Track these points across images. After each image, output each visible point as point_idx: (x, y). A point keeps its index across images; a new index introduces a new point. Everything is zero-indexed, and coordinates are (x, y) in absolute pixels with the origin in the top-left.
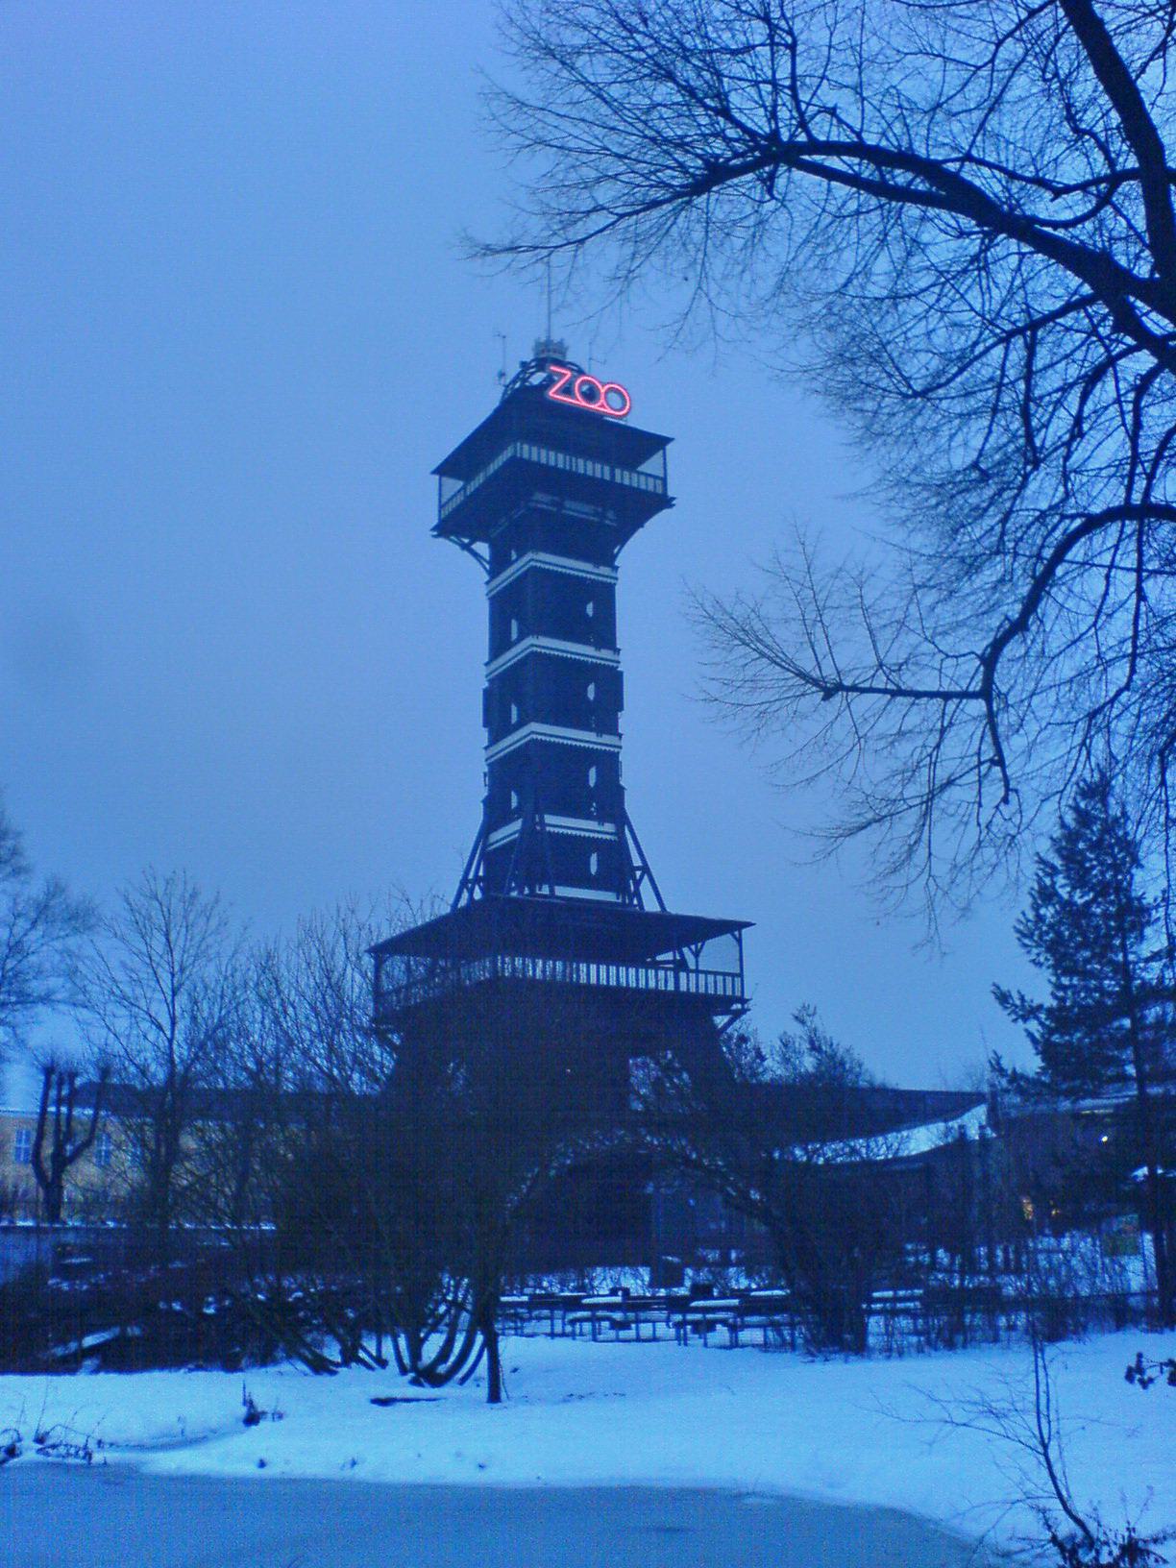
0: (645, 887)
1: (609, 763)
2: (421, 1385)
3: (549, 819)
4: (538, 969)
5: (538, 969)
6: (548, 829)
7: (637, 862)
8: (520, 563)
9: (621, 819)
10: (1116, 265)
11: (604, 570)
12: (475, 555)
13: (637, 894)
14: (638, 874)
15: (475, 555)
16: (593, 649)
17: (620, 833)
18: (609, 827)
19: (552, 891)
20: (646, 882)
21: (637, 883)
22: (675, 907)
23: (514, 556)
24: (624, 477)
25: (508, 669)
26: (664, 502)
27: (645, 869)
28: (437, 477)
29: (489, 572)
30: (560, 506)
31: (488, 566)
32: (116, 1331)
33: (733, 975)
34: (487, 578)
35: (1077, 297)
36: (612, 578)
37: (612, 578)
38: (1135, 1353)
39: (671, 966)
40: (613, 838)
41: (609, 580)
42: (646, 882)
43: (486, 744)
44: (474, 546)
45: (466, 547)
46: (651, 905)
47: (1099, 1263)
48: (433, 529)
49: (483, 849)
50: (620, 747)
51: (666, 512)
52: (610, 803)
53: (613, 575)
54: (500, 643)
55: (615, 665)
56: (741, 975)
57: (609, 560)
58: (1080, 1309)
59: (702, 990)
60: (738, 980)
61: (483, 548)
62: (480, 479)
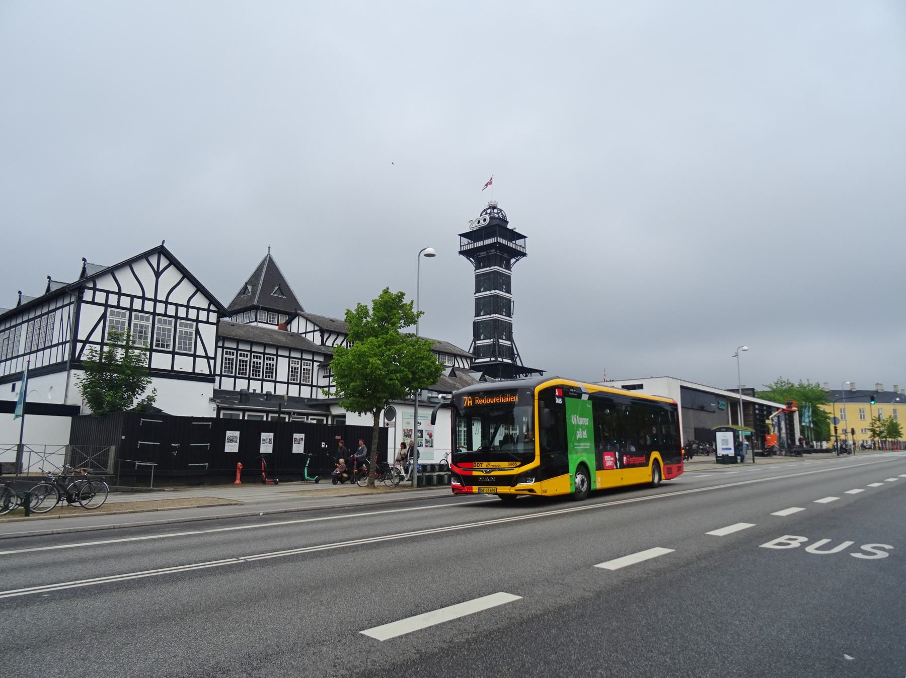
0: (518, 360)
2: (486, 381)
4: (308, 462)
5: (308, 462)
6: (500, 343)
7: (516, 353)
8: (484, 293)
13: (516, 361)
14: (516, 356)
17: (512, 345)
18: (510, 343)
20: (518, 358)
21: (516, 358)
22: (525, 365)
23: (482, 290)
24: (511, 245)
25: (487, 345)
26: (524, 255)
27: (518, 355)
29: (475, 267)
32: (306, 468)
38: (412, 299)
39: (570, 394)
42: (518, 358)
43: (474, 292)
45: (468, 259)
46: (519, 364)
49: (475, 347)
52: (510, 338)
54: (478, 291)
57: (508, 267)
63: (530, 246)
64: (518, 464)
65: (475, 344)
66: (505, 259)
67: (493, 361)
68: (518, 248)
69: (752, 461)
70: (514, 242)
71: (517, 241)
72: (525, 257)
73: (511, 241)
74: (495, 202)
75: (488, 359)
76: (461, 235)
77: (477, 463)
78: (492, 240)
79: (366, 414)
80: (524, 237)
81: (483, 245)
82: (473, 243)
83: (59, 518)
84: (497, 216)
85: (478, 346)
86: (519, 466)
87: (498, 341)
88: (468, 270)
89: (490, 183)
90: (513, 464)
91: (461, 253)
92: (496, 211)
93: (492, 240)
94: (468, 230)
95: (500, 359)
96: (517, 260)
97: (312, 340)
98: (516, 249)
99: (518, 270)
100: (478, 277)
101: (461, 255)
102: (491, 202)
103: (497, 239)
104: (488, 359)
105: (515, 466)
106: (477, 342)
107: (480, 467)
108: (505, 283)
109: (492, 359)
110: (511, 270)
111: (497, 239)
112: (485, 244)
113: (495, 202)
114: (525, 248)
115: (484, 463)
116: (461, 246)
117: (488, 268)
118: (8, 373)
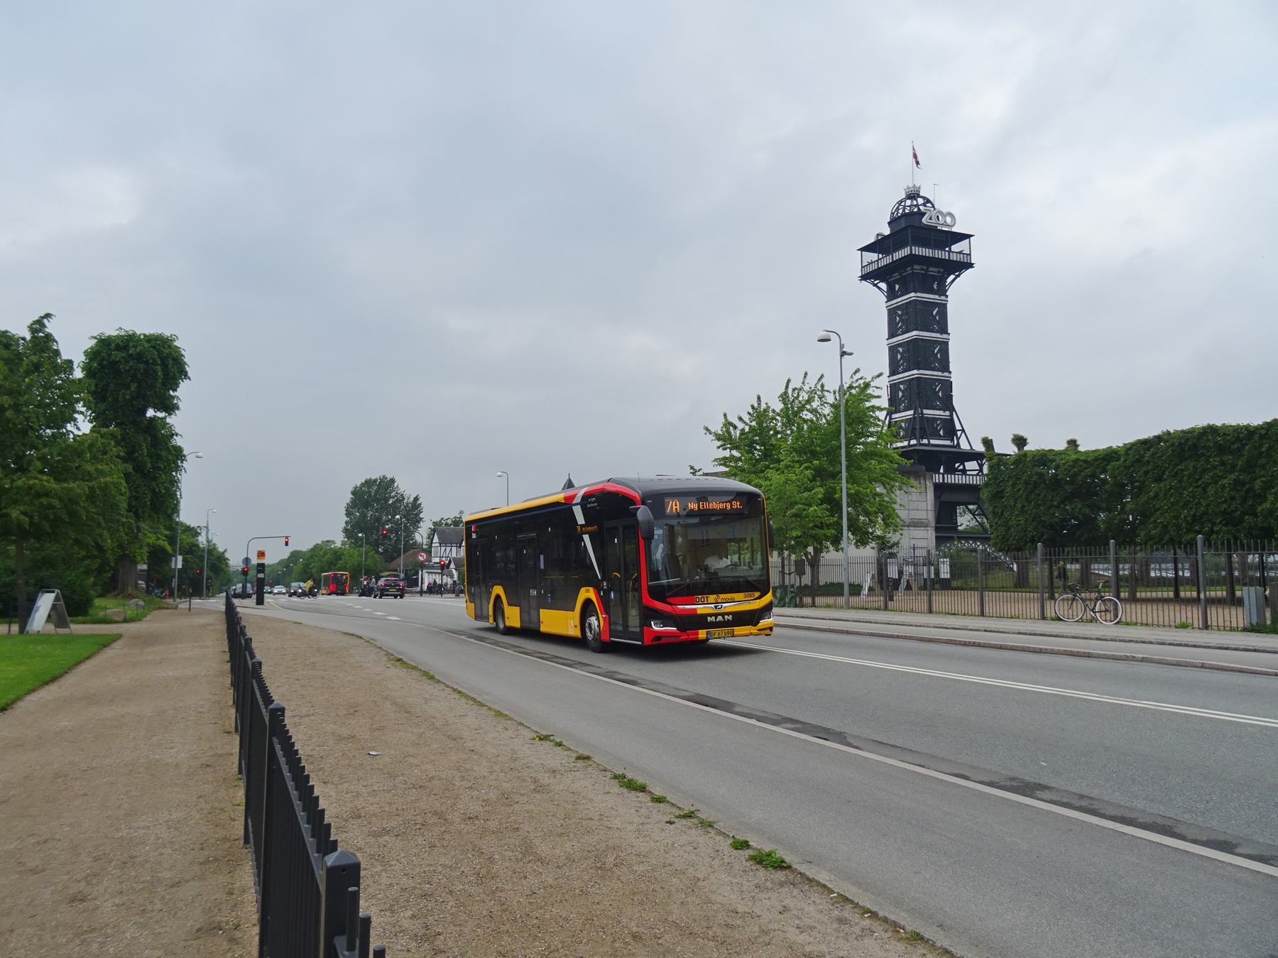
3: (925, 411)
7: (958, 427)
9: (952, 409)
10: (257, 589)
11: (943, 298)
12: (879, 288)
14: (959, 433)
15: (879, 288)
17: (951, 415)
18: (947, 413)
19: (929, 442)
24: (939, 254)
26: (970, 265)
27: (963, 431)
28: (860, 252)
30: (927, 271)
33: (967, 254)
34: (886, 300)
35: (957, 274)
45: (875, 285)
51: (970, 270)
52: (948, 404)
54: (892, 334)
56: (970, 255)
57: (942, 291)
60: (969, 256)
61: (883, 286)
63: (978, 250)
64: (757, 594)
66: (934, 278)
68: (954, 257)
69: (911, 537)
70: (947, 249)
73: (943, 249)
74: (914, 186)
75: (906, 443)
76: (863, 249)
77: (700, 597)
80: (968, 236)
82: (883, 258)
84: (916, 210)
85: (896, 422)
86: (759, 598)
88: (875, 300)
90: (750, 596)
91: (864, 277)
92: (920, 201)
94: (872, 240)
95: (925, 441)
96: (958, 276)
97: (969, 448)
98: (949, 260)
99: (959, 291)
100: (892, 313)
102: (908, 188)
103: (911, 249)
105: (752, 598)
107: (705, 602)
108: (936, 318)
109: (913, 442)
111: (911, 249)
112: (895, 259)
113: (914, 186)
115: (710, 596)
116: (862, 267)
117: (937, 297)
118: (1179, 623)
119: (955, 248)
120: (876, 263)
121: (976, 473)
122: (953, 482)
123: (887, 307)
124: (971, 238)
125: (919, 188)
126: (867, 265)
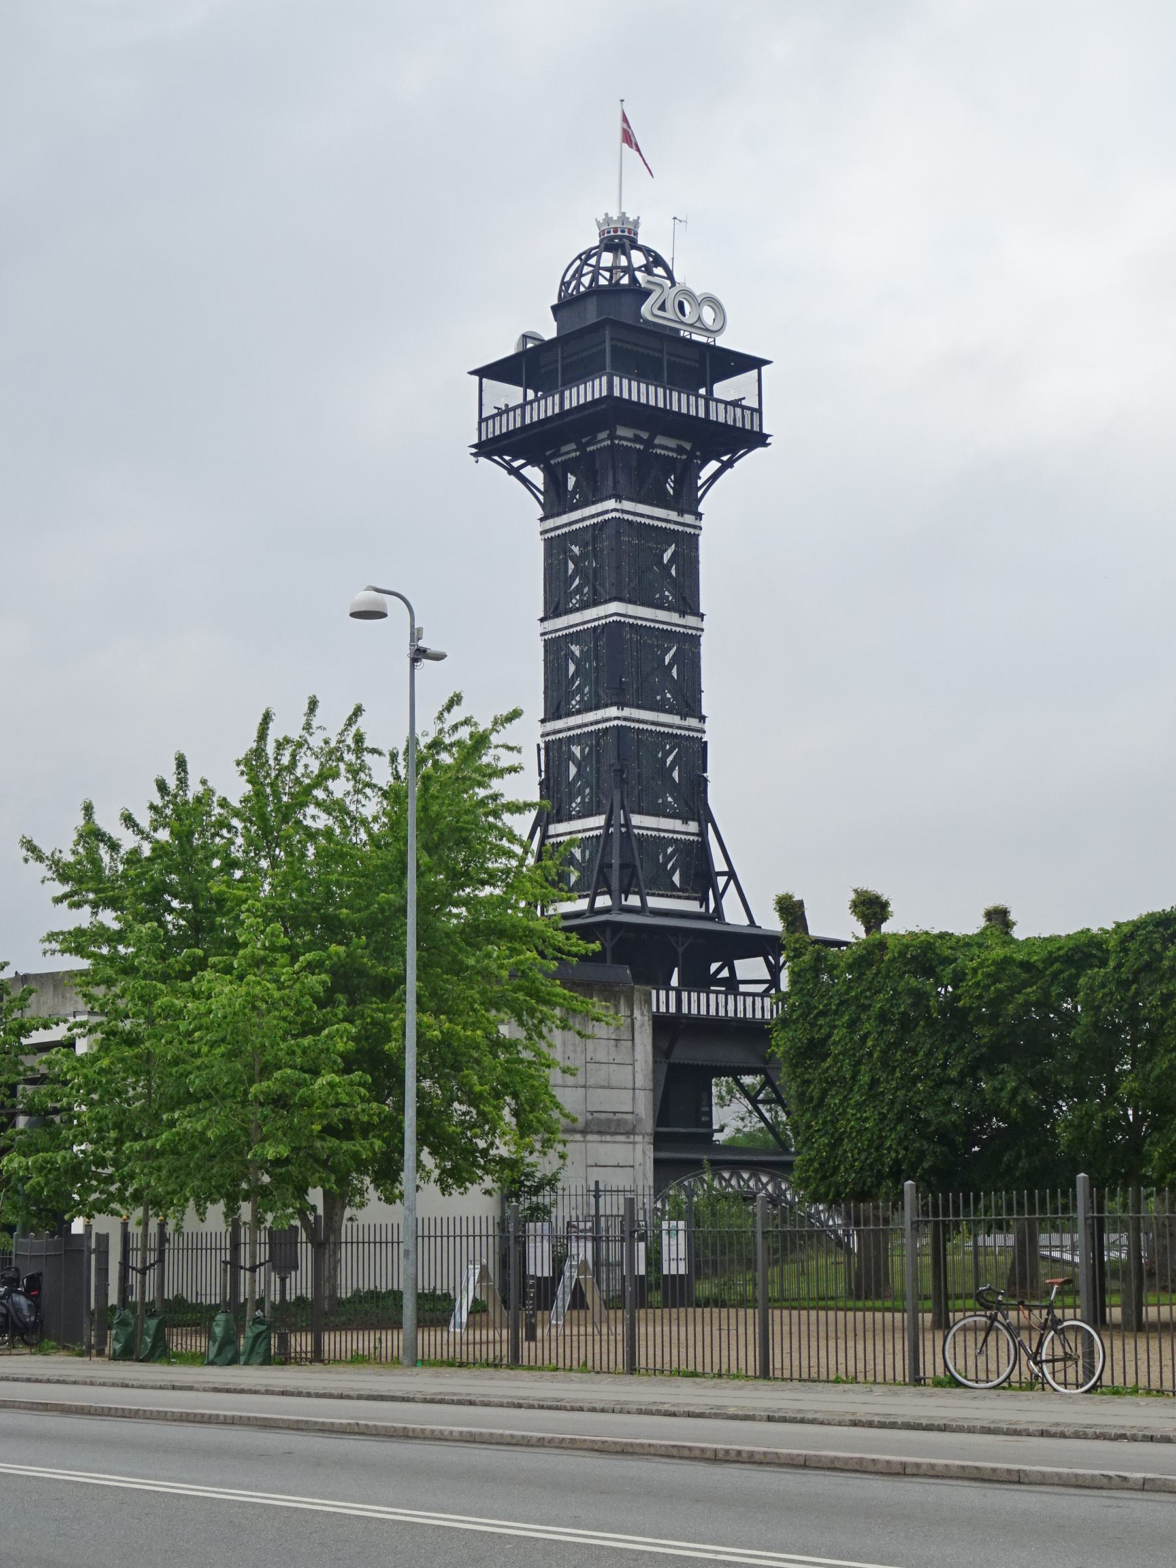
0: (731, 896)
1: (688, 544)
6: (636, 831)
7: (720, 865)
9: (704, 816)
11: (689, 519)
12: (524, 481)
14: (721, 881)
15: (524, 481)
16: (677, 615)
17: (703, 833)
18: (693, 827)
19: (643, 901)
26: (759, 439)
27: (731, 875)
28: (476, 378)
31: (541, 497)
36: (695, 527)
37: (695, 527)
40: (696, 838)
41: (694, 632)
44: (524, 472)
45: (515, 472)
47: (309, 956)
48: (767, 445)
50: (702, 630)
53: (697, 523)
54: (554, 607)
55: (699, 735)
58: (763, 1066)
59: (740, 1015)
61: (535, 475)
62: (680, 962)
65: (545, 836)
67: (606, 910)
68: (719, 415)
71: (717, 387)
72: (759, 450)
74: (623, 218)
76: (483, 373)
78: (592, 390)
79: (999, 918)
80: (757, 363)
81: (524, 428)
82: (537, 399)
83: (615, 1113)
84: (625, 281)
87: (628, 823)
89: (628, 138)
91: (485, 449)
92: (638, 258)
93: (592, 390)
95: (634, 900)
96: (729, 465)
100: (555, 548)
101: (483, 460)
102: (608, 220)
104: (582, 905)
106: (553, 829)
109: (603, 901)
110: (701, 509)
114: (759, 411)
116: (481, 420)
119: (725, 389)
120: (518, 411)
121: (760, 988)
122: (703, 1012)
123: (542, 533)
124: (764, 369)
125: (636, 223)
126: (493, 417)
